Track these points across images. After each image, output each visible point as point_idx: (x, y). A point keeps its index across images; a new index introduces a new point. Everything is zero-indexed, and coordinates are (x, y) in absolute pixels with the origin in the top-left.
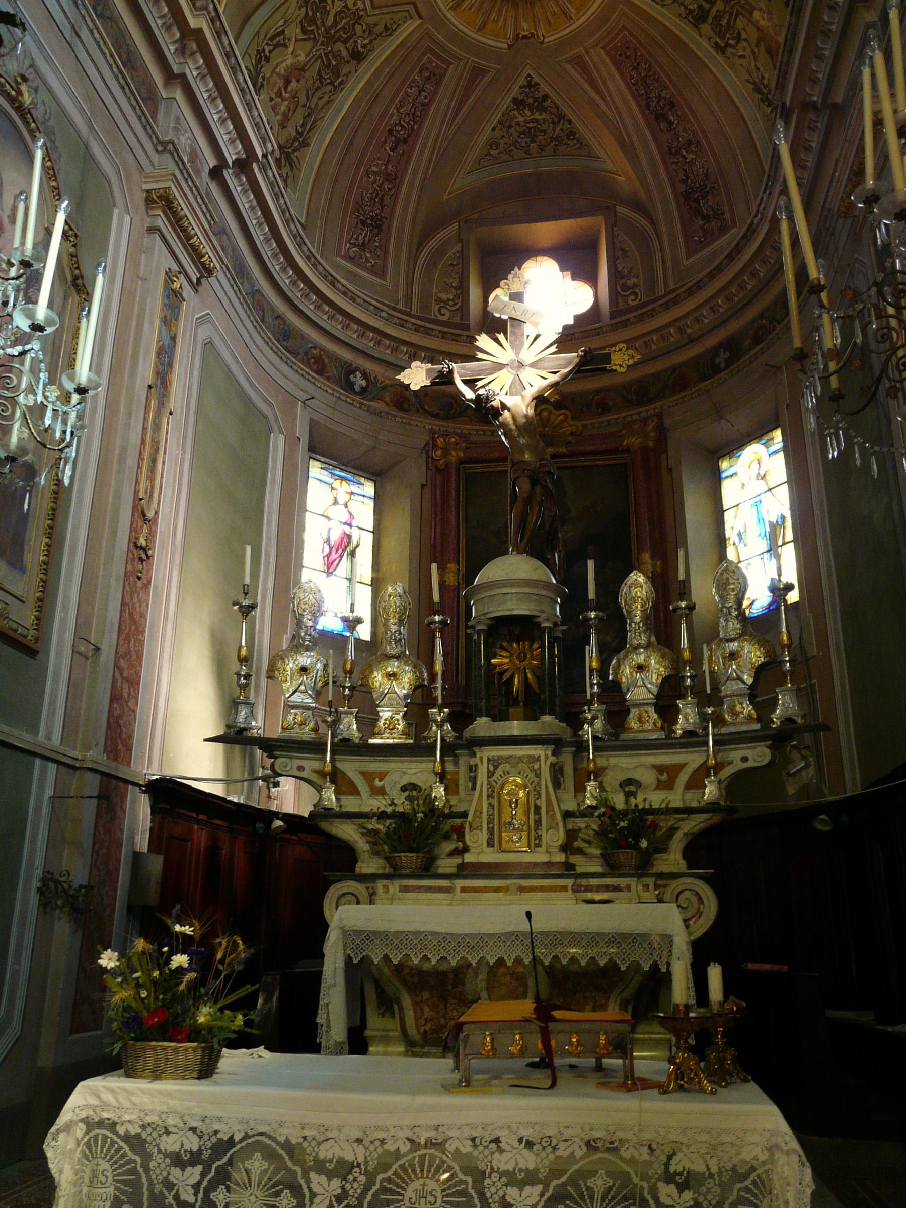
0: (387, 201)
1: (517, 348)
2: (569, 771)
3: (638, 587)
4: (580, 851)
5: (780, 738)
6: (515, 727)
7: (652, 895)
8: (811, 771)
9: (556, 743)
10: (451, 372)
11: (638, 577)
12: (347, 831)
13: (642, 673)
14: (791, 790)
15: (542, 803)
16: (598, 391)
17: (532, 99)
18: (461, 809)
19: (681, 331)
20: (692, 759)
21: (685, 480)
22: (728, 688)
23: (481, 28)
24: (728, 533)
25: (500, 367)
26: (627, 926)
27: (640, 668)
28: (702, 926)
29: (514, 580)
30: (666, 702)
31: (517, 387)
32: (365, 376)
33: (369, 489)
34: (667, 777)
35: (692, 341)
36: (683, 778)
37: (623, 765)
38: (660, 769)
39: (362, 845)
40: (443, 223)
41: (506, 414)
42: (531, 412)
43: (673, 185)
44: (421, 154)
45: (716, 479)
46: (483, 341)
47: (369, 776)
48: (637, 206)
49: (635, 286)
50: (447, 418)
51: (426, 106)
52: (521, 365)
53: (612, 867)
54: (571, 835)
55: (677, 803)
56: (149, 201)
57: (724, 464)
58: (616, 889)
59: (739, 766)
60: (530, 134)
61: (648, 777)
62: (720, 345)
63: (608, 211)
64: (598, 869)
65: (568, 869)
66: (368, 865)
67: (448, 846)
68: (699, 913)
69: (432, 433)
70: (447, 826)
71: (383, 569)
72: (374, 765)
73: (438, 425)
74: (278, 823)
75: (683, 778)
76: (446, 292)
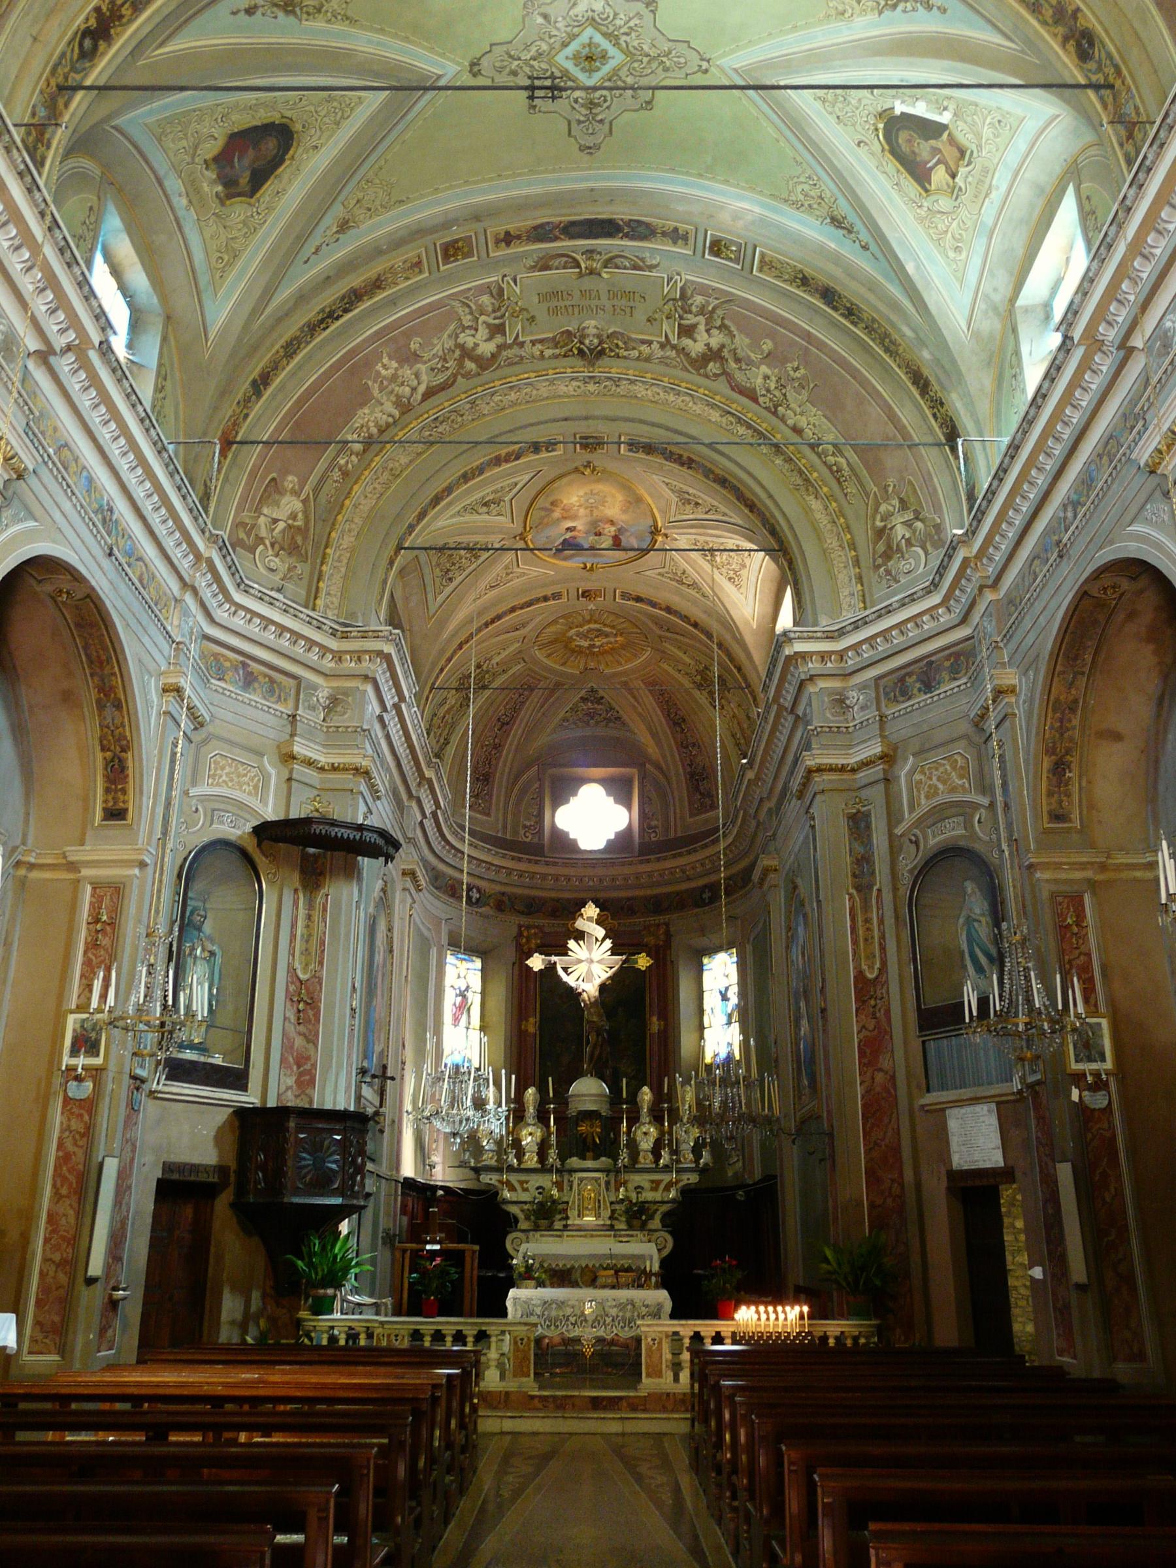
0: (494, 762)
1: (590, 950)
2: (613, 1181)
3: (646, 1095)
4: (616, 1219)
5: (703, 1171)
6: (589, 1164)
7: (646, 1239)
8: (740, 1164)
9: (607, 1171)
10: (555, 963)
11: (646, 1089)
12: (514, 1209)
13: (647, 1134)
14: (730, 1174)
15: (601, 1198)
16: (629, 899)
17: (593, 697)
18: (565, 1199)
19: (683, 872)
20: (666, 1178)
21: (681, 970)
22: (683, 1147)
23: (563, 664)
24: (705, 1007)
25: (580, 961)
26: (636, 1252)
27: (645, 1134)
28: (666, 1252)
29: (588, 1091)
30: (656, 1152)
31: (589, 977)
32: (479, 891)
33: (478, 964)
34: (655, 1185)
35: (689, 879)
36: (662, 1186)
37: (637, 1179)
38: (652, 1182)
39: (521, 1216)
40: (528, 767)
41: (585, 994)
42: (597, 994)
43: (683, 765)
44: (517, 731)
45: (700, 970)
46: (572, 944)
47: (521, 1183)
48: (658, 767)
49: (656, 827)
50: (529, 914)
51: (523, 703)
52: (592, 961)
53: (631, 1227)
54: (613, 1211)
55: (659, 1199)
56: (404, 874)
57: (706, 960)
58: (632, 1236)
59: (686, 1182)
60: (590, 715)
61: (647, 1185)
62: (705, 886)
63: (641, 766)
64: (625, 1227)
65: (612, 1228)
66: (524, 1225)
67: (559, 1217)
68: (665, 1247)
69: (520, 926)
70: (560, 1207)
71: (487, 1019)
72: (523, 1177)
73: (524, 920)
74: (441, 1192)
75: (662, 1186)
76: (529, 820)
